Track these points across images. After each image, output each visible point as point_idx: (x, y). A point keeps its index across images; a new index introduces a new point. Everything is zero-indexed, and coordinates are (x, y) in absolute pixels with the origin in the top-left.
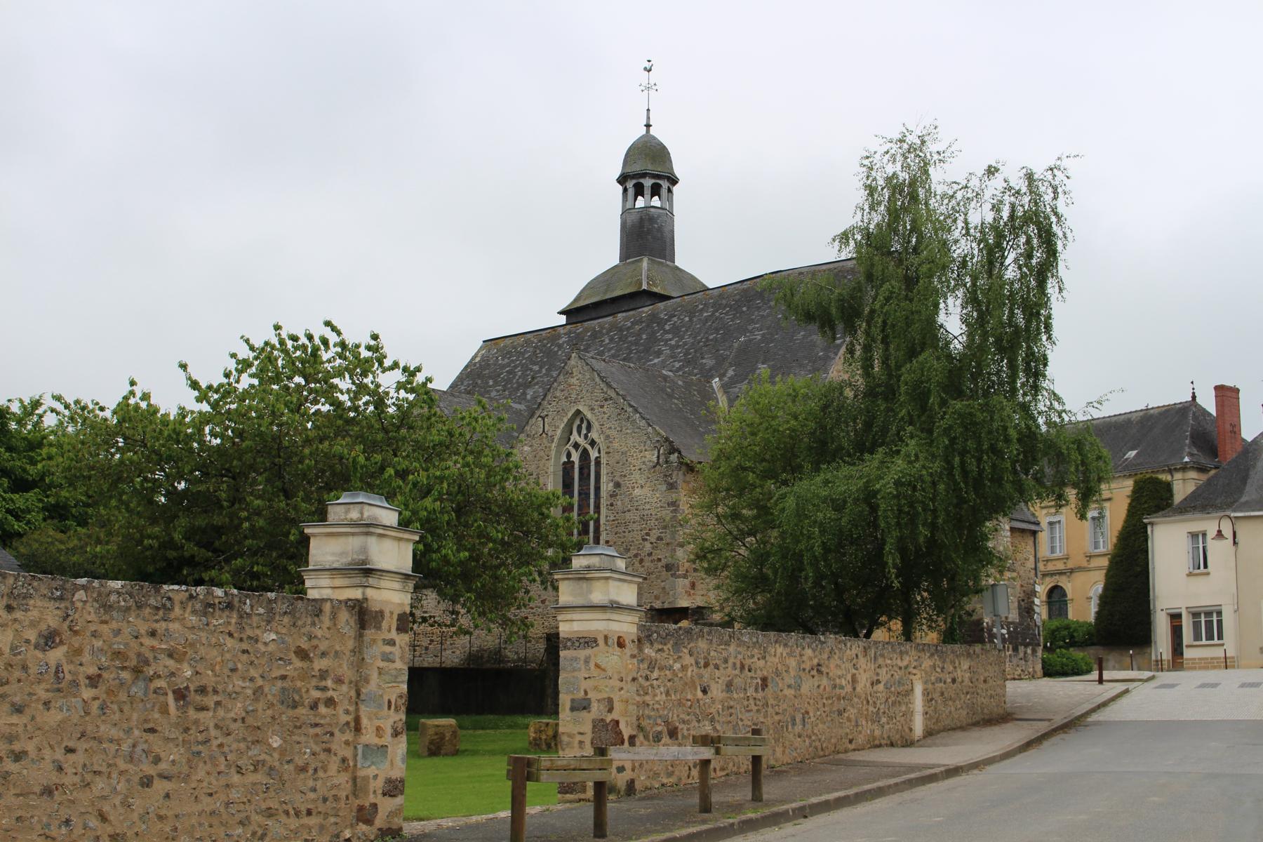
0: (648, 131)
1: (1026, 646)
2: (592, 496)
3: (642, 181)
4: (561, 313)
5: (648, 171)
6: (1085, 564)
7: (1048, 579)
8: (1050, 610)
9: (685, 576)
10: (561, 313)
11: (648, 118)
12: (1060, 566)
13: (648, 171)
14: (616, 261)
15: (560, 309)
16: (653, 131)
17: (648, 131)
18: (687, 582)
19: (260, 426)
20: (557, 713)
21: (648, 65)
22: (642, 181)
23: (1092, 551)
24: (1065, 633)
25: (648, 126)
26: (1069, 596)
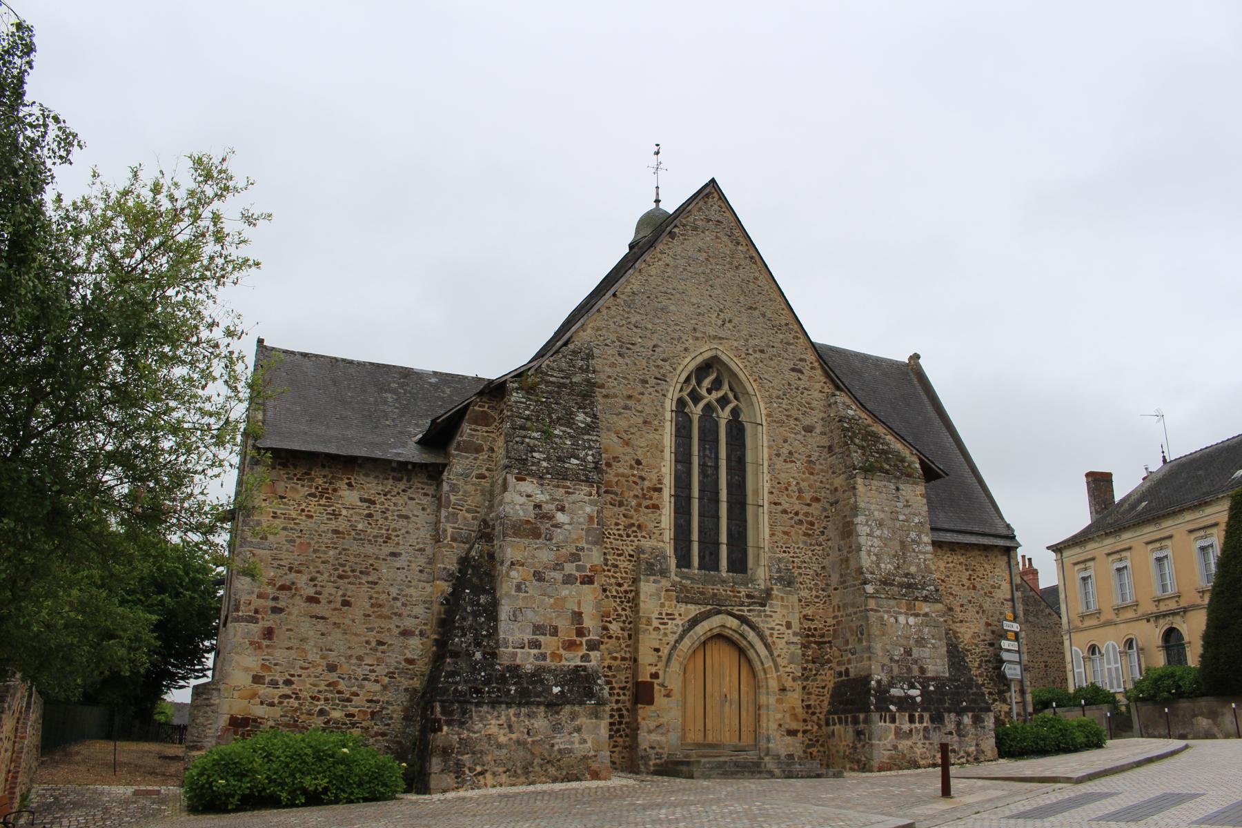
1: (960, 712)
6: (1113, 617)
7: (1161, 621)
8: (1168, 656)
12: (1172, 605)
16: (661, 206)
19: (102, 673)
20: (1002, 755)
21: (656, 149)
23: (1159, 593)
24: (1170, 682)
25: (657, 201)
26: (1186, 639)
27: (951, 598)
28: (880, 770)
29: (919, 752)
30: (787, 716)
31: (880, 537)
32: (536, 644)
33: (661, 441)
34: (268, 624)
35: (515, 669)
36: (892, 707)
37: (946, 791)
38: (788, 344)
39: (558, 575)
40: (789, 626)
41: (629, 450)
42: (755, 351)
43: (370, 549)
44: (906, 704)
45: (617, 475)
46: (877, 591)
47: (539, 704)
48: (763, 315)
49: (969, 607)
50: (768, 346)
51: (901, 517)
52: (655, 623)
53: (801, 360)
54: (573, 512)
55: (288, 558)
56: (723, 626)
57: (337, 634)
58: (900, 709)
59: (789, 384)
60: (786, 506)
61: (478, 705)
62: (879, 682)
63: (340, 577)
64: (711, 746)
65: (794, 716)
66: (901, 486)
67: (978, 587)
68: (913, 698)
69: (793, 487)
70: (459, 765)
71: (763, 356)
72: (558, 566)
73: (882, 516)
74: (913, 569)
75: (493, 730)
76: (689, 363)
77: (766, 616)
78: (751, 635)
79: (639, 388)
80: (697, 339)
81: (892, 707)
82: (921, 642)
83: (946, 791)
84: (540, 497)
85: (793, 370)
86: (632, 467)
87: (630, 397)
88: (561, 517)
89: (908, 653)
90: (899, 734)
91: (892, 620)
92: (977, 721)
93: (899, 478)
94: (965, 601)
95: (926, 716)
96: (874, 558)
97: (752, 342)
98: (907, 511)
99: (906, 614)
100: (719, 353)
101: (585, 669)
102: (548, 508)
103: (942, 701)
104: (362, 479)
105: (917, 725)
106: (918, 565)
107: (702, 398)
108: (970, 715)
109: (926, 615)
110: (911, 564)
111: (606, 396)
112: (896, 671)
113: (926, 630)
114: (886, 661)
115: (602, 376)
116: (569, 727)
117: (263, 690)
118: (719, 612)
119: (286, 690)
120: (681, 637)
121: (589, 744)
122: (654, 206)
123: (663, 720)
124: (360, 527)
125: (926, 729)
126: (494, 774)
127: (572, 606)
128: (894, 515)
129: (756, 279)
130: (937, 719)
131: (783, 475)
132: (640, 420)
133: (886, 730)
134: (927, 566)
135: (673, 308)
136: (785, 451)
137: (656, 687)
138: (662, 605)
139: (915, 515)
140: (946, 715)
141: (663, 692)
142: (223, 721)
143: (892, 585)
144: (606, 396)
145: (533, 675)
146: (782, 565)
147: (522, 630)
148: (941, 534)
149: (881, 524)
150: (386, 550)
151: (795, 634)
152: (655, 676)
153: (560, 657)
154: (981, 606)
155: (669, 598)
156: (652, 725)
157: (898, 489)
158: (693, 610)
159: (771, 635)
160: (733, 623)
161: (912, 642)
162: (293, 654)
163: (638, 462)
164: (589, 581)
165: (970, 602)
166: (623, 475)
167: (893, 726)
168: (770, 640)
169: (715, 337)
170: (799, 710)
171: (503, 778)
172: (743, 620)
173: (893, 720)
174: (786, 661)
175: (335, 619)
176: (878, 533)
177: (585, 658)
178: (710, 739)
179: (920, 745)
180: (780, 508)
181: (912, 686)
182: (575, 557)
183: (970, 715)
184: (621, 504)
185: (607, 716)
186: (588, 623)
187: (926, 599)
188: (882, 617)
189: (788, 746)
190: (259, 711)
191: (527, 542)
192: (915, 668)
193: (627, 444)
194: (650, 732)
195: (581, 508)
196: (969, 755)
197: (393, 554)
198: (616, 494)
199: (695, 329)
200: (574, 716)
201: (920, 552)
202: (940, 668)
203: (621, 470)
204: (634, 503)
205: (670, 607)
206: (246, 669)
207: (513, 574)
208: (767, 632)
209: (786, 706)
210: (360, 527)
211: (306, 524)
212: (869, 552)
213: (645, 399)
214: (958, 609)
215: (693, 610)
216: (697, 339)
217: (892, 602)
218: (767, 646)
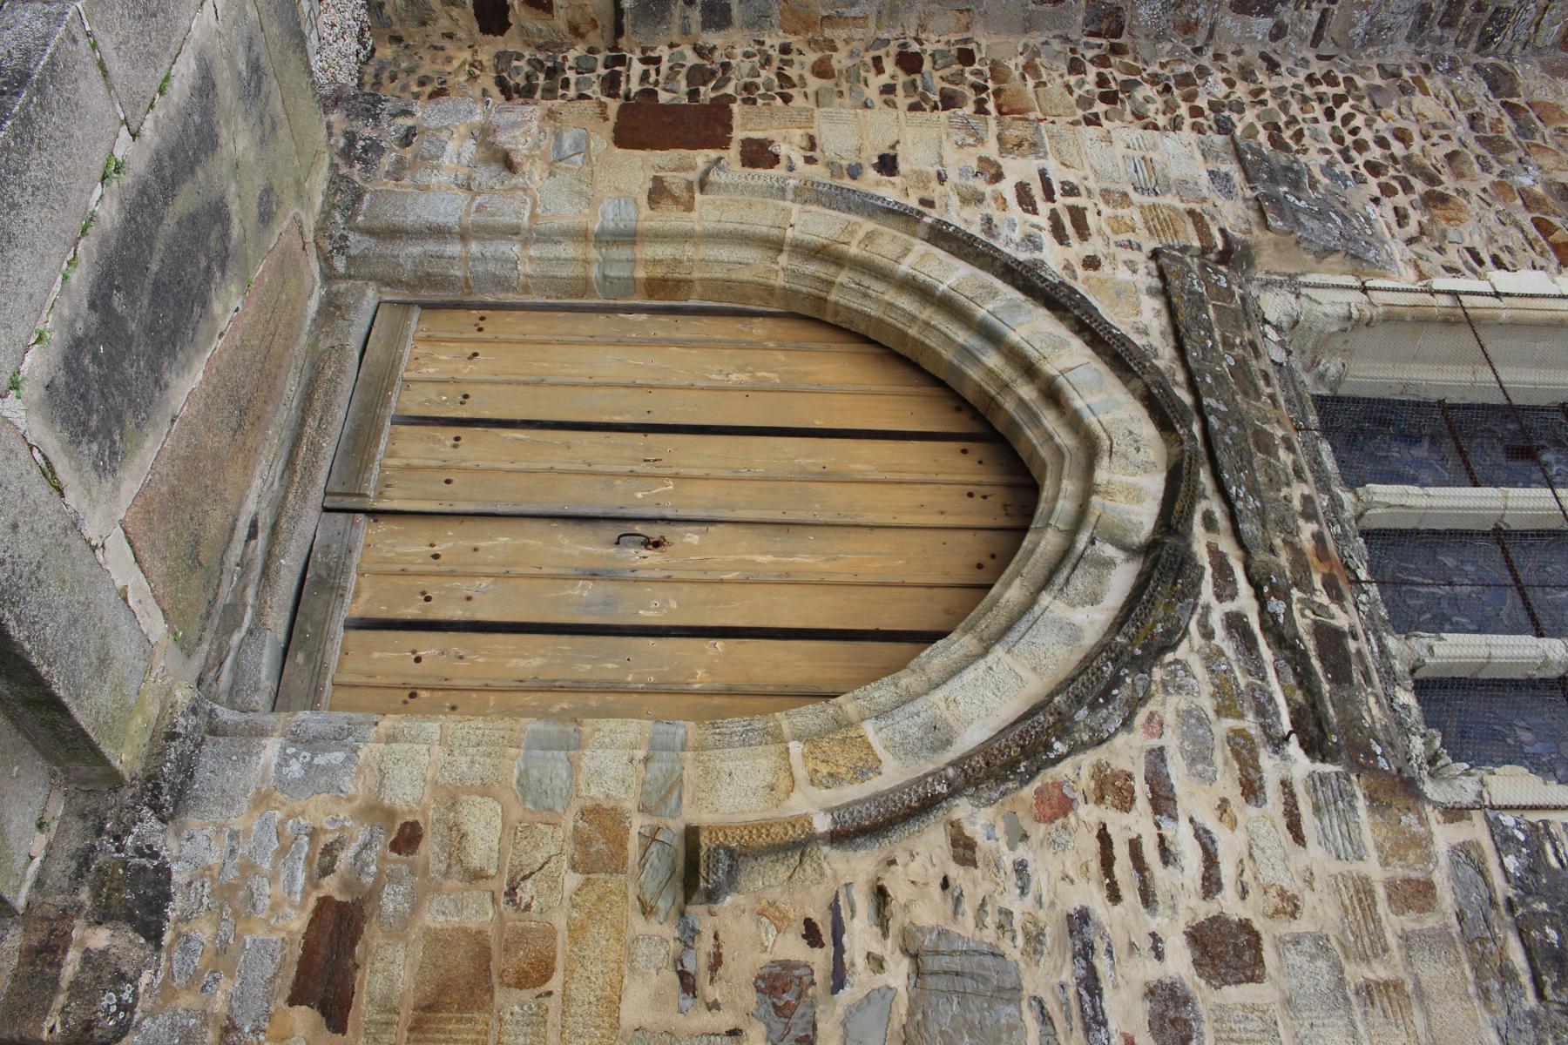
30: (480, 913)
52: (1019, 169)
56: (1091, 448)
78: (1082, 616)
120: (946, 238)
123: (534, 174)
137: (702, 157)
141: (675, 180)
148: (629, 525)
152: (759, 155)
155: (1157, 221)
158: (1141, 319)
159: (1114, 789)
168: (1074, 772)
172: (1164, 561)
174: (927, 912)
189: (233, 897)
205: (1118, 225)
208: (1126, 752)
209: (557, 898)
215: (1141, 319)
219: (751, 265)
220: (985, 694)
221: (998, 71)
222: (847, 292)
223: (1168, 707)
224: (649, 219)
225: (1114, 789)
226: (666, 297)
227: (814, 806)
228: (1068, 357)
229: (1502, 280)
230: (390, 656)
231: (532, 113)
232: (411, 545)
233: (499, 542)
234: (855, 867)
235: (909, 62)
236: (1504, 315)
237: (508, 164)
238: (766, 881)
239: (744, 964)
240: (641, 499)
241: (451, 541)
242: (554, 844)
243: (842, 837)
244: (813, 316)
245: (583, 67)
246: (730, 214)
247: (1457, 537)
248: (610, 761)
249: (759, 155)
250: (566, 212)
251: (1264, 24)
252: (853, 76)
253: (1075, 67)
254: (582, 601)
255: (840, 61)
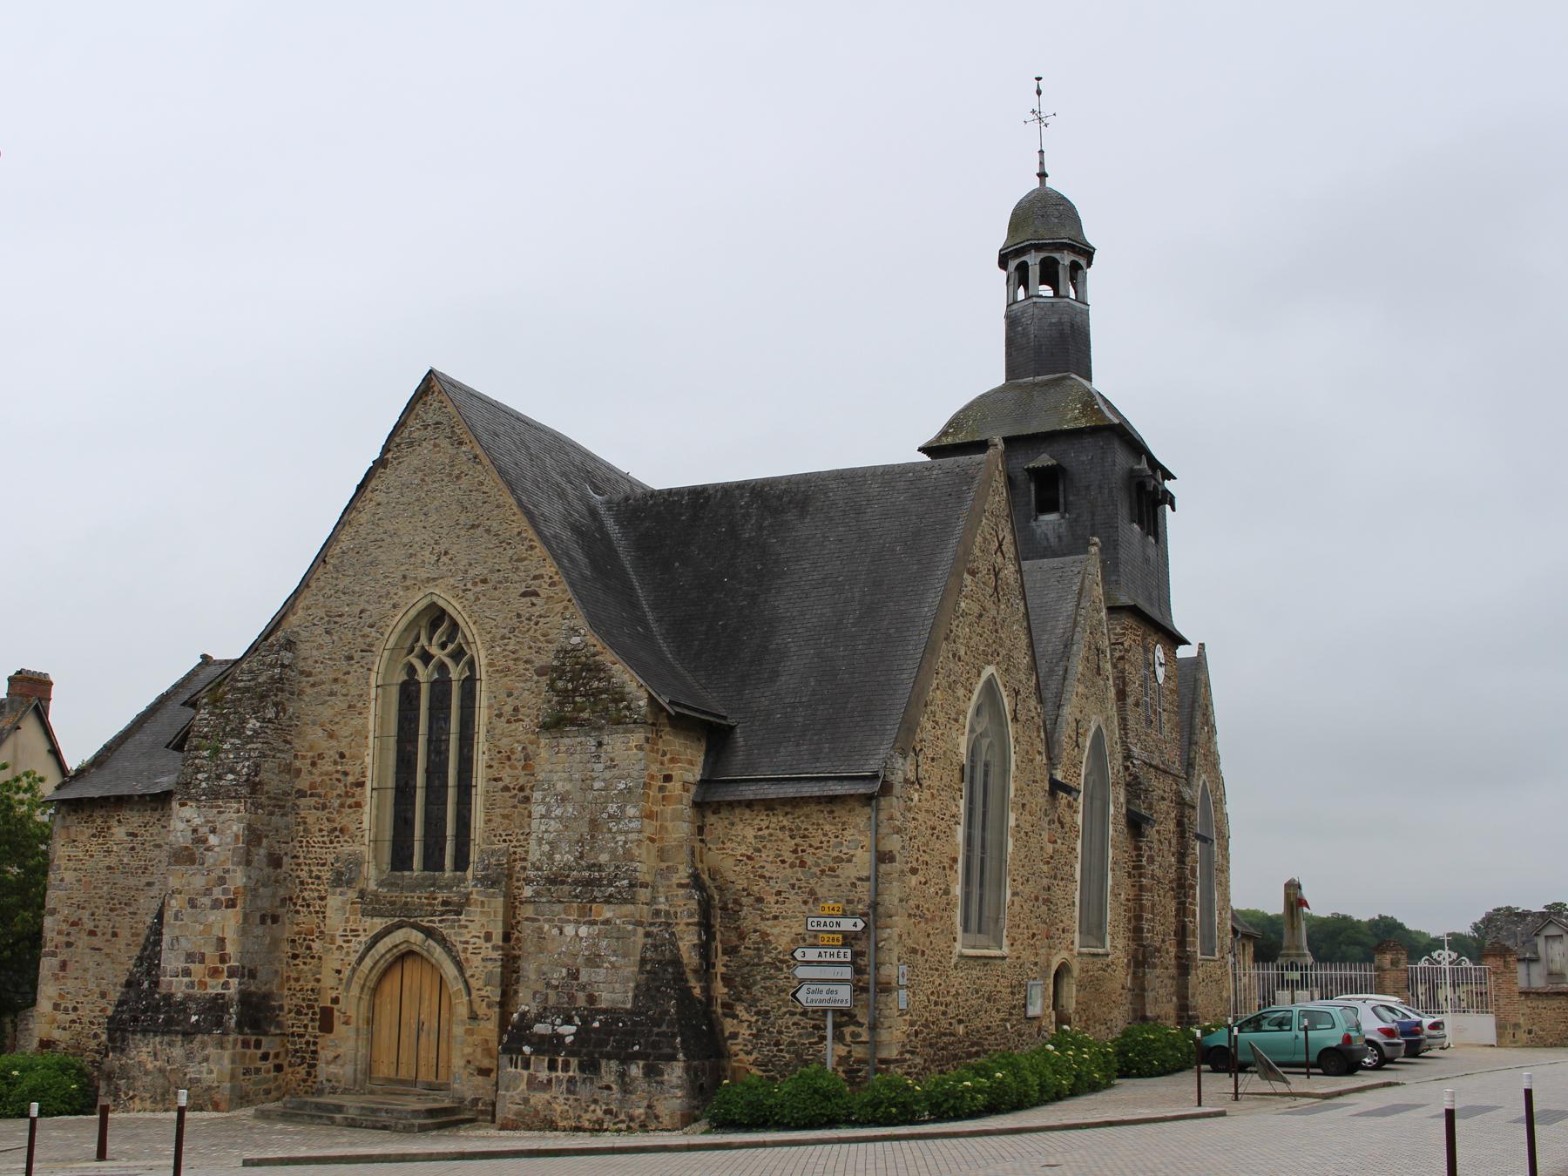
0: (1043, 183)
1: (627, 1059)
2: (451, 794)
3: (1057, 256)
4: (922, 450)
5: (1046, 246)
9: (54, 954)
10: (922, 450)
11: (1042, 163)
13: (1046, 246)
14: (998, 378)
15: (922, 444)
16: (1049, 183)
17: (1043, 183)
18: (55, 961)
22: (1057, 256)
25: (1042, 175)
27: (762, 883)
28: (503, 1128)
29: (559, 1109)
30: (479, 1050)
31: (560, 818)
32: (187, 973)
33: (365, 726)
34: (64, 957)
35: (168, 997)
36: (527, 1049)
37: (102, 1154)
38: (520, 560)
39: (207, 901)
40: (488, 937)
41: (334, 743)
42: (475, 584)
43: (132, 882)
44: (550, 1046)
45: (321, 774)
46: (537, 894)
47: (177, 1033)
48: (488, 531)
49: (792, 895)
50: (491, 572)
51: (597, 785)
52: (339, 941)
53: (535, 578)
54: (223, 833)
55: (79, 896)
57: (108, 964)
58: (536, 1052)
59: (519, 616)
60: (507, 781)
61: (134, 1032)
62: (523, 1015)
63: (111, 910)
64: (402, 1082)
65: (488, 1052)
66: (606, 739)
67: (809, 860)
68: (562, 1037)
69: (519, 755)
70: (118, 1089)
71: (485, 587)
72: (208, 892)
73: (568, 787)
74: (604, 858)
75: (144, 1057)
76: (399, 621)
77: (461, 927)
78: (438, 951)
79: (344, 665)
80: (408, 588)
81: (527, 1049)
82: (594, 961)
83: (102, 1154)
84: (197, 821)
85: (524, 595)
86: (335, 763)
87: (336, 680)
88: (213, 840)
89: (574, 975)
90: (533, 1083)
91: (555, 931)
92: (651, 1072)
93: (600, 729)
94: (784, 886)
95: (574, 1062)
96: (546, 848)
97: (472, 572)
98: (608, 774)
99: (577, 922)
100: (435, 598)
101: (223, 996)
102: (203, 830)
103: (602, 1043)
104: (128, 814)
105: (560, 1073)
106: (613, 852)
107: (432, 657)
108: (641, 1063)
109: (607, 922)
110: (602, 850)
111: (313, 685)
112: (553, 999)
113: (604, 943)
114: (540, 986)
115: (310, 662)
116: (199, 1057)
117: (60, 1016)
118: (399, 926)
119: (73, 1016)
120: (361, 960)
121: (214, 1075)
122: (1035, 183)
123: (340, 1051)
124: (125, 860)
125: (571, 1080)
126: (142, 1099)
127: (217, 932)
128: (586, 783)
129: (481, 484)
130: (590, 1067)
131: (505, 741)
132: (345, 706)
133: (517, 1077)
134: (627, 852)
135: (383, 557)
136: (508, 709)
137: (336, 1013)
138: (347, 920)
139: (621, 777)
140: (604, 1063)
142: (35, 1043)
143: (563, 882)
144: (313, 685)
145: (181, 1003)
146: (493, 860)
147: (177, 960)
149: (563, 799)
150: (144, 880)
151: (495, 948)
152: (336, 1000)
153: (205, 984)
154: (812, 893)
155: (354, 912)
156: (331, 1055)
157: (600, 744)
158: (379, 923)
159: (465, 950)
160: (417, 937)
161: (580, 960)
162: (79, 983)
163: (342, 756)
164: (231, 904)
165: (793, 886)
166: (327, 774)
167: (525, 1073)
168: (462, 956)
169: (428, 580)
170: (494, 1044)
171: (148, 1104)
172: (429, 933)
173: (526, 1066)
175: (106, 950)
176: (558, 812)
177: (226, 985)
178: (403, 1074)
179: (561, 1100)
180: (501, 784)
181: (568, 1021)
182: (222, 880)
183: (641, 1063)
184: (324, 807)
185: (230, 1046)
186: (230, 949)
187: (608, 900)
188: (541, 928)
189: (476, 1088)
190: (57, 1034)
191: (183, 868)
192: (581, 996)
193: (331, 736)
194: (328, 1063)
195: (230, 827)
196: (632, 1119)
197: (149, 884)
198: (320, 796)
199: (404, 577)
200: (204, 1046)
201: (620, 832)
202: (619, 997)
203: (325, 768)
204: (336, 803)
206: (50, 998)
207: (173, 902)
208: (460, 947)
209: (477, 1038)
210: (125, 860)
211: (89, 864)
212: (540, 841)
213: (351, 679)
214: (772, 899)
215: (379, 923)
216: (408, 588)
217: (558, 907)
218: (459, 965)
219: (364, 1004)
220: (450, 970)
221: (299, 933)
222: (371, 984)
223: (453, 938)
224: (353, 1025)
225: (465, 950)
226: (370, 1021)
227: (466, 999)
228: (387, 942)
229: (366, 825)
230: (442, 1072)
231: (321, 1053)
232: (423, 1070)
233: (422, 1053)
234: (474, 993)
235: (295, 956)
236: (374, 812)
237: (337, 1057)
238: (476, 1007)
239: (487, 1011)
240: (414, 1026)
241: (422, 1062)
242: (470, 1039)
243: (469, 994)
244: (375, 991)
245: (294, 1043)
246: (352, 1004)
247: (430, 728)
248: (458, 1030)
249: (336, 1000)
250: (352, 1043)
251: (285, 859)
252: (301, 972)
253: (298, 912)
254: (434, 1036)
255: (294, 975)
